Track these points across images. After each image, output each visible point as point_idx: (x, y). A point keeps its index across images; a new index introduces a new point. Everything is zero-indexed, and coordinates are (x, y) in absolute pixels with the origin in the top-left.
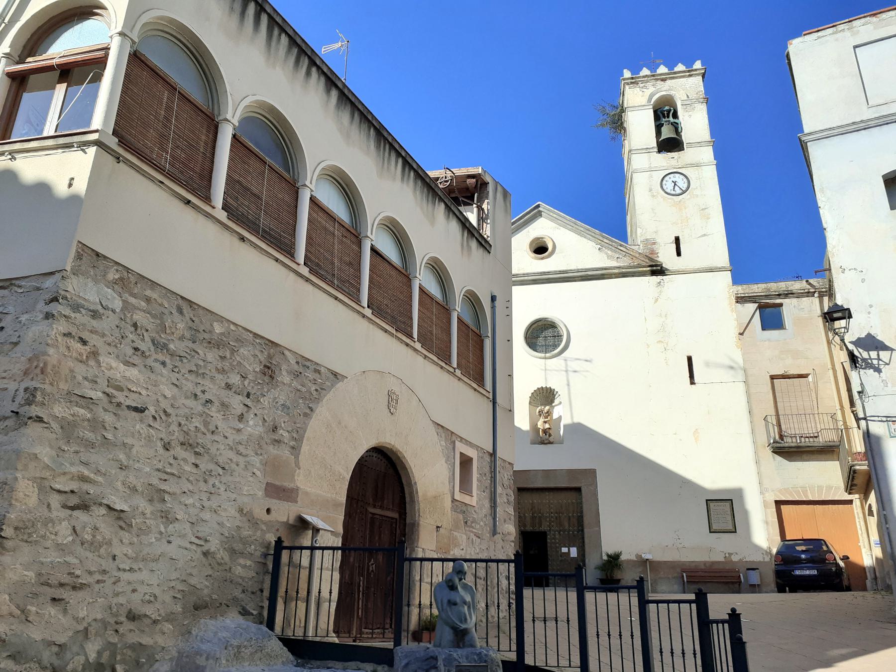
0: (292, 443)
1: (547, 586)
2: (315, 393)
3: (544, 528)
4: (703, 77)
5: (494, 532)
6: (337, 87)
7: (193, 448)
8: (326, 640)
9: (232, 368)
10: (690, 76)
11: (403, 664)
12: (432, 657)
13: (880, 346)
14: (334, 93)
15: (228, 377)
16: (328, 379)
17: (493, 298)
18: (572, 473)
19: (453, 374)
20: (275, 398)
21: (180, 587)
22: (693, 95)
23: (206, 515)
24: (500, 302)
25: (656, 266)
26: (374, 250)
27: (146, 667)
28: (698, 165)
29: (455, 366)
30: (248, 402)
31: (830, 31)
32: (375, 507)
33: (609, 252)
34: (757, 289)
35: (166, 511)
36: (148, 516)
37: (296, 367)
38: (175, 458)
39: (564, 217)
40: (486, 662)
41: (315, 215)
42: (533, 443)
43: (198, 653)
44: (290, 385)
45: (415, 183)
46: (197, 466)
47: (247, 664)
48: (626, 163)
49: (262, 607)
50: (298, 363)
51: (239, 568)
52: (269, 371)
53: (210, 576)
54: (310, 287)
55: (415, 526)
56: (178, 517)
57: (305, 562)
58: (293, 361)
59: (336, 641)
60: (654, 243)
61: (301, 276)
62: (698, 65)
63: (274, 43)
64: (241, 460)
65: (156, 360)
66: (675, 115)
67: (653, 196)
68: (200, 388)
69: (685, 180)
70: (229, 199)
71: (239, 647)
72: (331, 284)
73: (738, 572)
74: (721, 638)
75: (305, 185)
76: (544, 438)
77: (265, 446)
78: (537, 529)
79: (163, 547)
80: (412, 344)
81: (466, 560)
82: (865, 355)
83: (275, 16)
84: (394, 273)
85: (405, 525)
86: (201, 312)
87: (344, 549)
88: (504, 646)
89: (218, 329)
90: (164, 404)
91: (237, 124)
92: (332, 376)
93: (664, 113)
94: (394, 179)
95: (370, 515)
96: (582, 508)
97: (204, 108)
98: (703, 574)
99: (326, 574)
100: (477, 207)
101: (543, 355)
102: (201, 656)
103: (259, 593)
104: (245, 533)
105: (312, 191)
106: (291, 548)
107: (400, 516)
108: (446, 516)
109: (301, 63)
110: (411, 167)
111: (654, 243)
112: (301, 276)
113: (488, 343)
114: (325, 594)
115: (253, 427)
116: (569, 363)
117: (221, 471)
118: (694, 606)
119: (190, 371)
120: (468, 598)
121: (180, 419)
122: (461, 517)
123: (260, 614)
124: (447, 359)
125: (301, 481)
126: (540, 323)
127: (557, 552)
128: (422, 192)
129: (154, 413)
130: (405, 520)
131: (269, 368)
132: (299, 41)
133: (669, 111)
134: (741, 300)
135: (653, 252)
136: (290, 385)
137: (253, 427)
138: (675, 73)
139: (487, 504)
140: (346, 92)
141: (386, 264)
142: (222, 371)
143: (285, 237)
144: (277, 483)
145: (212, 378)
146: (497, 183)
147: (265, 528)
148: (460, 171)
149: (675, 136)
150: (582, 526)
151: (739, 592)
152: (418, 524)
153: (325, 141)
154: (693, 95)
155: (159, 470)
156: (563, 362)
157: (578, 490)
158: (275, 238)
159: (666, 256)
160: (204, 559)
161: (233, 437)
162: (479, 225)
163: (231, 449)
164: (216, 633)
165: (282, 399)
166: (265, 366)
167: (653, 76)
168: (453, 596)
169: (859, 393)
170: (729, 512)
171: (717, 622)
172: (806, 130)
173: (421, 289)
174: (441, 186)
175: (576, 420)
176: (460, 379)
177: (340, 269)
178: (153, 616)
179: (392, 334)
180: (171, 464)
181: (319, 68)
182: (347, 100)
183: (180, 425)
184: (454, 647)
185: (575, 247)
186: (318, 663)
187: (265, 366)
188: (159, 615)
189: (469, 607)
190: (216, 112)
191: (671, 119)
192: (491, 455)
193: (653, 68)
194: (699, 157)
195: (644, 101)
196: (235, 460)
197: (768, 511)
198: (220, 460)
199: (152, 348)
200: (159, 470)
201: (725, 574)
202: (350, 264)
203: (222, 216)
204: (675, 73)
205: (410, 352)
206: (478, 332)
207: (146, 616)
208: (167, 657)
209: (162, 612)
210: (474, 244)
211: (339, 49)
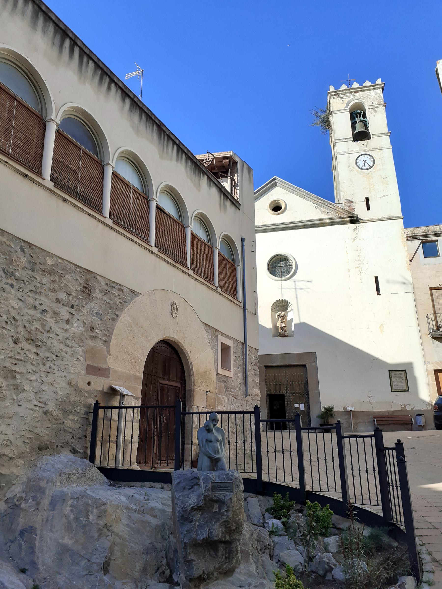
0: (104, 338)
1: (285, 429)
2: (119, 305)
3: (283, 391)
4: (383, 90)
5: (246, 395)
6: (129, 97)
7: (35, 342)
8: (131, 468)
9: (60, 289)
10: (374, 89)
11: (176, 483)
12: (196, 478)
14: (128, 101)
15: (58, 295)
16: (128, 295)
17: (242, 240)
18: (300, 355)
19: (216, 291)
20: (91, 308)
21: (28, 435)
23: (45, 387)
24: (247, 243)
25: (353, 217)
26: (158, 208)
27: (5, 489)
28: (380, 149)
29: (217, 285)
30: (73, 311)
32: (164, 379)
33: (322, 209)
34: (420, 230)
35: (17, 385)
36: (4, 388)
37: (105, 287)
38: (22, 349)
40: (231, 480)
41: (116, 184)
42: (274, 336)
43: (42, 479)
44: (102, 299)
45: (186, 162)
46: (38, 354)
47: (75, 485)
48: (332, 149)
49: (86, 448)
50: (107, 284)
51: (70, 421)
52: (86, 291)
53: (50, 427)
54: (113, 233)
55: (192, 391)
56: (25, 388)
57: (115, 416)
58: (103, 283)
59: (139, 468)
60: (352, 202)
61: (107, 225)
62: (379, 81)
63: (84, 67)
64: (69, 350)
65: (6, 284)
66: (365, 116)
67: (351, 170)
68: (38, 302)
70: (55, 174)
71: (69, 474)
72: (129, 231)
73: (411, 417)
74: (391, 458)
75: (108, 164)
76: (281, 333)
77: (85, 341)
78: (278, 392)
79: (16, 409)
80: (187, 271)
81: (218, 413)
83: (84, 48)
84: (172, 223)
85: (185, 391)
86: (37, 250)
87: (144, 408)
88: (249, 469)
89: (50, 262)
90: (13, 313)
91: (59, 123)
92: (131, 293)
93: (357, 114)
94: (171, 159)
95: (161, 385)
96: (307, 378)
97: (36, 111)
98: (388, 419)
99: (129, 425)
100: (230, 179)
102: (43, 480)
103: (84, 438)
104: (73, 398)
105: (113, 167)
106: (105, 408)
107: (181, 386)
108: (213, 385)
109: (103, 81)
110: (182, 151)
111: (352, 202)
112: (107, 225)
113: (239, 270)
114: (128, 437)
115: (76, 327)
116: (297, 283)
117: (55, 358)
118: (373, 439)
119: (31, 291)
120: (220, 438)
121: (25, 323)
122: (223, 385)
123: (85, 452)
124: (211, 280)
125: (112, 363)
126: (277, 257)
127: (292, 407)
128: (191, 168)
129: (6, 319)
130: (185, 387)
131: (86, 288)
132: (101, 65)
134: (410, 238)
135: (351, 208)
136: (102, 299)
137: (76, 327)
139: (240, 376)
140: (136, 100)
141: (167, 217)
142: (53, 290)
143: (95, 200)
144: (94, 365)
145: (46, 295)
146: (243, 162)
147: (87, 395)
150: (308, 390)
151: (411, 430)
152: (194, 390)
153: (121, 133)
155: (10, 357)
157: (305, 366)
158: (88, 200)
159: (360, 210)
160: (45, 416)
161: (62, 334)
162: (232, 190)
163: (61, 342)
164: (53, 466)
165: (96, 309)
166: (84, 287)
167: (349, 89)
168: (210, 436)
170: (404, 378)
171: (388, 449)
173: (192, 234)
174: (206, 165)
175: (302, 321)
176: (220, 294)
177: (135, 221)
178: (9, 455)
179: (172, 265)
180: (19, 353)
181: (116, 84)
182: (137, 105)
183: (25, 327)
184: (210, 470)
185: (300, 206)
186: (125, 483)
187: (84, 287)
188: (14, 454)
189: (221, 444)
190: (44, 115)
191: (362, 118)
192: (243, 344)
193: (349, 84)
194: (381, 144)
195: (344, 107)
196: (64, 350)
197: (430, 376)
198: (54, 350)
199: (4, 275)
200: (10, 357)
202: (142, 217)
203: (50, 185)
204: (364, 87)
205: (186, 276)
206: (232, 262)
207: (4, 455)
208: (20, 482)
209: (16, 452)
210: (228, 203)
211: (137, 76)
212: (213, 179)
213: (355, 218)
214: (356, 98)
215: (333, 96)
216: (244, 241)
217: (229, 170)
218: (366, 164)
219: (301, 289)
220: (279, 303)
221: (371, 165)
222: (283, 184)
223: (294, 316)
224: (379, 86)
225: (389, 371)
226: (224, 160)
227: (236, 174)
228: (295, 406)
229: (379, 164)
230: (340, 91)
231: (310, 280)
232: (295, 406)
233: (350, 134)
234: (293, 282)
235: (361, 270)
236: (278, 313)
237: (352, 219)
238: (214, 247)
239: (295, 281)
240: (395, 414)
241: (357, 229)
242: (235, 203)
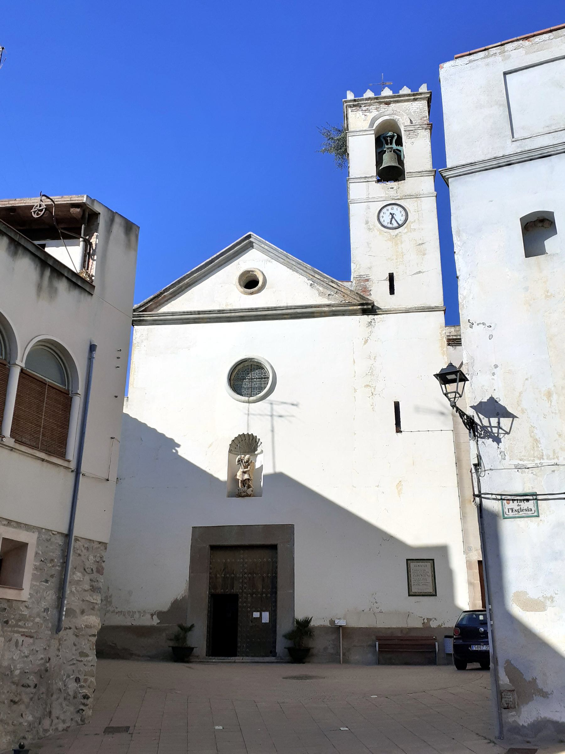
3: (236, 590)
5: (58, 628)
10: (415, 100)
13: (500, 412)
18: (268, 528)
22: (416, 121)
25: (367, 304)
28: (417, 197)
31: (482, 54)
33: (321, 289)
39: (275, 250)
42: (231, 495)
60: (367, 280)
62: (423, 88)
66: (399, 142)
69: (403, 212)
78: (228, 591)
82: (485, 422)
93: (387, 138)
101: (246, 399)
111: (367, 280)
116: (275, 407)
126: (246, 364)
133: (392, 137)
135: (366, 290)
138: (399, 96)
139: (50, 596)
148: (59, 200)
149: (397, 165)
150: (276, 588)
154: (416, 121)
156: (269, 406)
157: (274, 547)
159: (379, 295)
167: (377, 98)
169: (475, 465)
170: (430, 574)
172: (449, 165)
175: (278, 470)
176: (12, 449)
185: (287, 282)
191: (394, 146)
193: (377, 91)
195: (366, 125)
201: (424, 642)
204: (399, 96)
212: (23, 242)
213: (370, 307)
214: (387, 113)
215: (350, 107)
216: (94, 350)
217: (83, 226)
218: (393, 220)
219: (281, 416)
220: (244, 439)
221: (400, 223)
222: (263, 245)
223: (265, 462)
224: (423, 96)
225: (407, 560)
226: (72, 210)
227: (96, 234)
228: (254, 616)
229: (415, 221)
230: (363, 100)
231: (295, 403)
232: (254, 616)
233: (373, 171)
234: (269, 405)
235: (373, 390)
236: (239, 457)
237: (365, 307)
238: (12, 362)
239: (271, 404)
240: (413, 634)
241: (373, 324)
242: (79, 283)
